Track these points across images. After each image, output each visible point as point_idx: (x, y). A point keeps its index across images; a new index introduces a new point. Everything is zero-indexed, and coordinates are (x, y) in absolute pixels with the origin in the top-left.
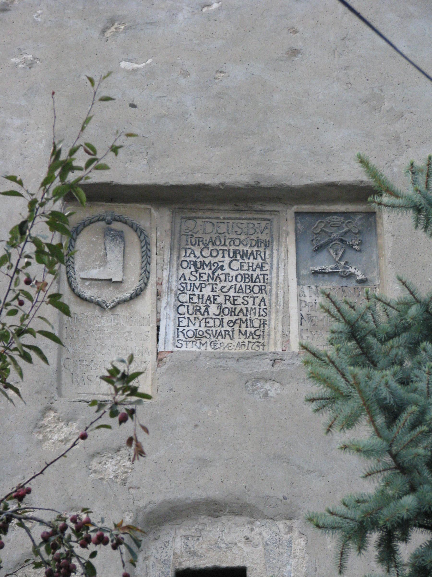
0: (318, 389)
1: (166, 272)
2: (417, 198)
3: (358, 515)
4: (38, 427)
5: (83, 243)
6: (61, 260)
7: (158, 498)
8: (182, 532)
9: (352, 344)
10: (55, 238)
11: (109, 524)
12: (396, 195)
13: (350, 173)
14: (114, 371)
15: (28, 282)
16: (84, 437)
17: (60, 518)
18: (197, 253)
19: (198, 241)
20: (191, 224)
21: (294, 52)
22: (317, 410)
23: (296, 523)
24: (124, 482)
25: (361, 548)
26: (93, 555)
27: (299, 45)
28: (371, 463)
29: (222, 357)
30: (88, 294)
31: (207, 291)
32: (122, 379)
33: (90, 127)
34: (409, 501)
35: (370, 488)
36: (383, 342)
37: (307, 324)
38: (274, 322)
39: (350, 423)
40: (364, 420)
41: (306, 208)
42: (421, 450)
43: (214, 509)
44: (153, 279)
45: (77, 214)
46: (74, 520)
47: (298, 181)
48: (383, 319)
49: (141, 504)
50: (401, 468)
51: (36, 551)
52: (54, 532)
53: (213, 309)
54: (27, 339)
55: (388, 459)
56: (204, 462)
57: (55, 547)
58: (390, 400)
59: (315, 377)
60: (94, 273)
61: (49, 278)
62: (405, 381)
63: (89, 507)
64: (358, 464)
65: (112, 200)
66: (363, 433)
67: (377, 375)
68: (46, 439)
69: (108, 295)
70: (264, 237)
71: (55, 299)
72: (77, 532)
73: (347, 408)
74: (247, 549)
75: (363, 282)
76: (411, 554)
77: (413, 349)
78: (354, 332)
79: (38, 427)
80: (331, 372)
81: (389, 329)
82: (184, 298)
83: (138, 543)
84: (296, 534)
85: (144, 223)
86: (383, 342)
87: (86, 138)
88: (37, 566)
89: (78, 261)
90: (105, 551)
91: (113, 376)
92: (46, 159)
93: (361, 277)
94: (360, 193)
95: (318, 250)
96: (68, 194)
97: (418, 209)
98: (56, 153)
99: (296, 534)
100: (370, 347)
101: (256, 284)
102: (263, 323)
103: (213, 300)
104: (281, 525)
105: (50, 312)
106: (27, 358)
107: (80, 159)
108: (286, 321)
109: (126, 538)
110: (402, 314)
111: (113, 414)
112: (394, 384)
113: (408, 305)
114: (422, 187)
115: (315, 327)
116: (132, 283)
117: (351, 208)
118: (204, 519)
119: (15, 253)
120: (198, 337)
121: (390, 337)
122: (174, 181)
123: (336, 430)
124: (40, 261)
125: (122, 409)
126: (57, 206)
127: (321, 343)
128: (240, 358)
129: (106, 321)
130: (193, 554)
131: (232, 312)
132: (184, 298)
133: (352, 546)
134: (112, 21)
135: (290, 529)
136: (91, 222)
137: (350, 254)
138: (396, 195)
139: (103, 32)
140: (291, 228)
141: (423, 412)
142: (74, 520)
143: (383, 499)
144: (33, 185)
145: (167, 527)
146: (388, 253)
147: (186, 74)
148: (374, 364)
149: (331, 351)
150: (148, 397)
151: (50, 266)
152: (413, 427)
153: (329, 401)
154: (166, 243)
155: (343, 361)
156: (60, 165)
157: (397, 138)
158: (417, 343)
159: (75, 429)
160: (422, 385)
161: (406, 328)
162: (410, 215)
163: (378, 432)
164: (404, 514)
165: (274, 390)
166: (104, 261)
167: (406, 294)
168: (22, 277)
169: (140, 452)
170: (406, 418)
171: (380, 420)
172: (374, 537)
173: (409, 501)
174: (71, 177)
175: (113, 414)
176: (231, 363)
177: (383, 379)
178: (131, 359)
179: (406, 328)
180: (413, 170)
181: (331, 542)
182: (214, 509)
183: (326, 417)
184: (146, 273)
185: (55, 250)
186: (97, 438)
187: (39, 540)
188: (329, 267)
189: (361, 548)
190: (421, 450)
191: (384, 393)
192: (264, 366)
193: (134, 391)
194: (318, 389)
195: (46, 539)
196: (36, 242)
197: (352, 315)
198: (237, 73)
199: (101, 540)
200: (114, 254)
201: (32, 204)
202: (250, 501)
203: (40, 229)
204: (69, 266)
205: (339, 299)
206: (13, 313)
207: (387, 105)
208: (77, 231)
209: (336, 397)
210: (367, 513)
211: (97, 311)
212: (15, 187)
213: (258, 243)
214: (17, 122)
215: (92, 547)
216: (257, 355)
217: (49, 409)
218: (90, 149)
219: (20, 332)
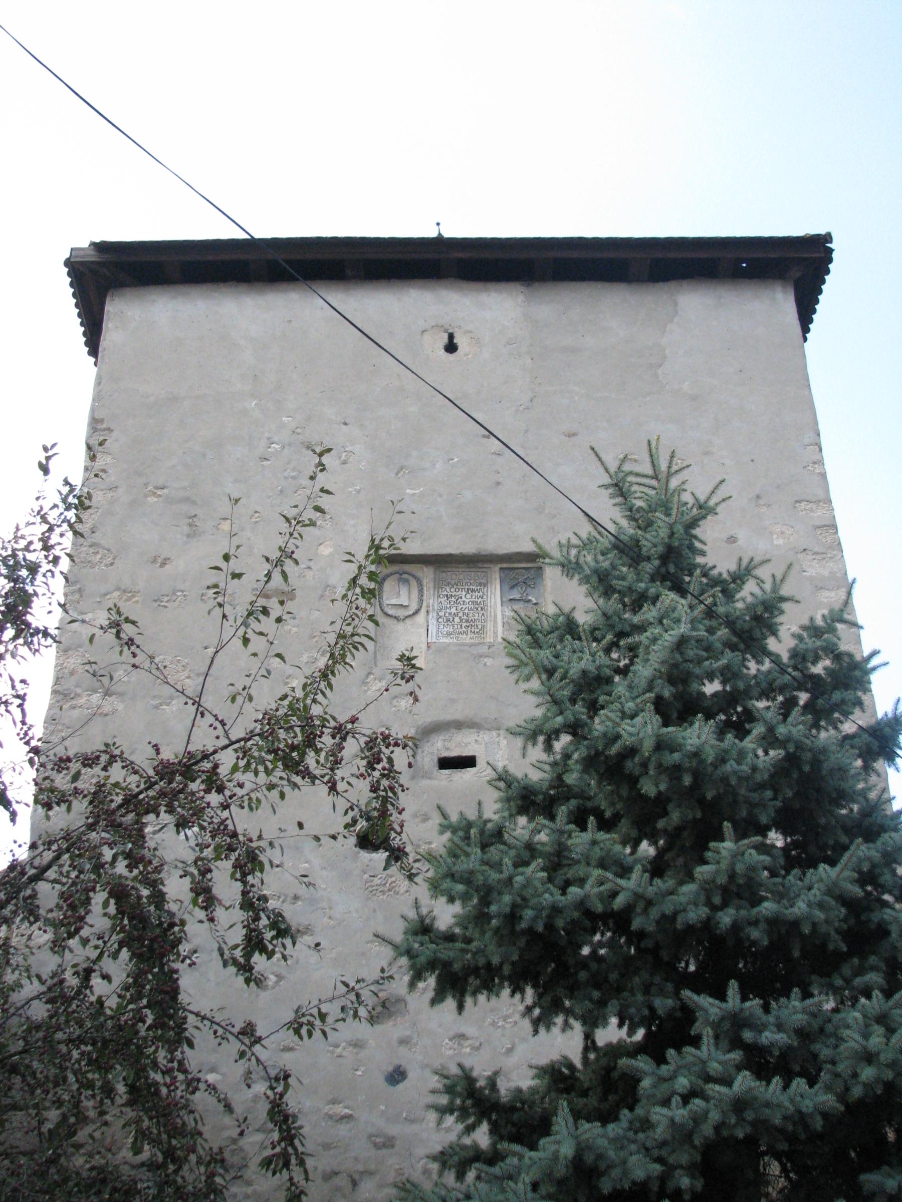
0: (511, 661)
1: (431, 600)
2: (562, 559)
3: (533, 727)
4: (364, 683)
5: (387, 586)
6: (375, 596)
7: (428, 720)
8: (442, 737)
9: (529, 637)
10: (372, 585)
11: (400, 736)
12: (551, 558)
13: (527, 547)
14: (403, 656)
15: (357, 608)
16: (387, 690)
17: (374, 733)
18: (447, 590)
19: (449, 584)
20: (444, 575)
21: (498, 483)
22: (740, 559)
23: (502, 732)
24: (410, 712)
25: (534, 744)
26: (392, 752)
27: (501, 480)
28: (540, 700)
29: (463, 645)
30: (390, 612)
31: (453, 610)
32: (407, 660)
33: (391, 527)
34: (559, 719)
35: (539, 713)
36: (545, 636)
37: (506, 627)
38: (489, 626)
39: (528, 679)
40: (535, 676)
41: (505, 565)
42: (565, 693)
43: (459, 725)
44: (425, 604)
45: (383, 570)
46: (382, 734)
47: (501, 551)
48: (545, 623)
49: (420, 723)
50: (556, 702)
51: (362, 750)
52: (371, 741)
53: (457, 620)
54: (356, 639)
55: (549, 698)
56: (453, 701)
57: (372, 748)
58: (549, 666)
59: (510, 655)
60: (394, 601)
61: (368, 606)
62: (557, 656)
63: (707, 541)
64: (533, 700)
65: (402, 563)
66: (535, 683)
67: (542, 652)
68: (369, 689)
69: (401, 613)
70: (483, 581)
71: (371, 618)
72: (384, 740)
73: (526, 671)
74: (476, 746)
75: (535, 604)
76: (714, 732)
77: (561, 639)
78: (530, 631)
79: (364, 683)
80: (518, 652)
81: (548, 629)
82: (442, 614)
83: (416, 746)
84: (502, 737)
85: (419, 574)
86: (545, 636)
87: (390, 532)
88: (362, 759)
89: (385, 596)
90: (398, 750)
91: (402, 658)
92: (368, 544)
93: (534, 601)
94: (531, 557)
95: (512, 587)
96: (378, 560)
97: (563, 566)
98: (373, 541)
99: (502, 737)
100: (538, 638)
101: (480, 607)
102: (483, 627)
103: (456, 615)
104: (494, 733)
105: (370, 625)
106: (356, 648)
107: (386, 544)
108: (495, 626)
109: (410, 744)
110: (556, 620)
111: (402, 678)
112: (551, 658)
113: (559, 616)
114: (565, 553)
115: (511, 628)
116: (414, 606)
117: (529, 565)
118: (453, 730)
119: (350, 593)
120: (449, 634)
121: (550, 633)
122: (435, 552)
123: (520, 682)
124: (363, 597)
125: (407, 676)
126: (373, 568)
127: (512, 638)
128: (471, 645)
129: (400, 627)
130: (447, 749)
131: (467, 621)
132: (442, 614)
133: (530, 744)
134: (402, 468)
135: (499, 735)
136: (391, 574)
137: (529, 590)
138: (551, 558)
139: (397, 474)
140: (497, 576)
141: (566, 672)
142: (382, 734)
143: (546, 718)
144: (360, 556)
145: (433, 735)
146: (549, 589)
147: (441, 496)
148: (541, 648)
149: (518, 641)
150: (421, 669)
151: (369, 600)
152: (561, 680)
153: (516, 668)
154: (431, 585)
155: (524, 646)
156: (375, 546)
157: (553, 528)
158: (563, 636)
159: (383, 684)
160: (566, 658)
161: (557, 629)
162: (560, 568)
163: (542, 683)
164: (557, 726)
165: (489, 661)
166: (398, 595)
167: (557, 611)
168: (354, 606)
169: (416, 700)
170: (557, 675)
171: (544, 676)
172: (541, 739)
173: (559, 719)
174: (382, 552)
175: (402, 678)
176: (467, 648)
177: (545, 655)
178: (412, 649)
179: (557, 629)
180: (560, 545)
181: (519, 742)
182: (459, 725)
183: (515, 676)
184: (421, 601)
185: (372, 591)
186: (394, 690)
187: (363, 745)
188: (518, 597)
189: (534, 744)
190: (565, 693)
191: (546, 662)
192: (484, 649)
193: (413, 666)
194: (511, 661)
195: (367, 743)
196: (361, 587)
197: (529, 621)
198: (468, 495)
199: (396, 744)
200: (404, 591)
201: (360, 567)
202: (477, 720)
203: (363, 580)
204: (381, 598)
205: (523, 615)
206: (349, 624)
207: (547, 511)
208: (384, 579)
209: (522, 664)
210: (537, 726)
211: (395, 621)
212: (351, 558)
213: (480, 584)
214: (352, 522)
215: (391, 748)
216: (480, 644)
217: (370, 673)
218: (391, 539)
219: (353, 635)
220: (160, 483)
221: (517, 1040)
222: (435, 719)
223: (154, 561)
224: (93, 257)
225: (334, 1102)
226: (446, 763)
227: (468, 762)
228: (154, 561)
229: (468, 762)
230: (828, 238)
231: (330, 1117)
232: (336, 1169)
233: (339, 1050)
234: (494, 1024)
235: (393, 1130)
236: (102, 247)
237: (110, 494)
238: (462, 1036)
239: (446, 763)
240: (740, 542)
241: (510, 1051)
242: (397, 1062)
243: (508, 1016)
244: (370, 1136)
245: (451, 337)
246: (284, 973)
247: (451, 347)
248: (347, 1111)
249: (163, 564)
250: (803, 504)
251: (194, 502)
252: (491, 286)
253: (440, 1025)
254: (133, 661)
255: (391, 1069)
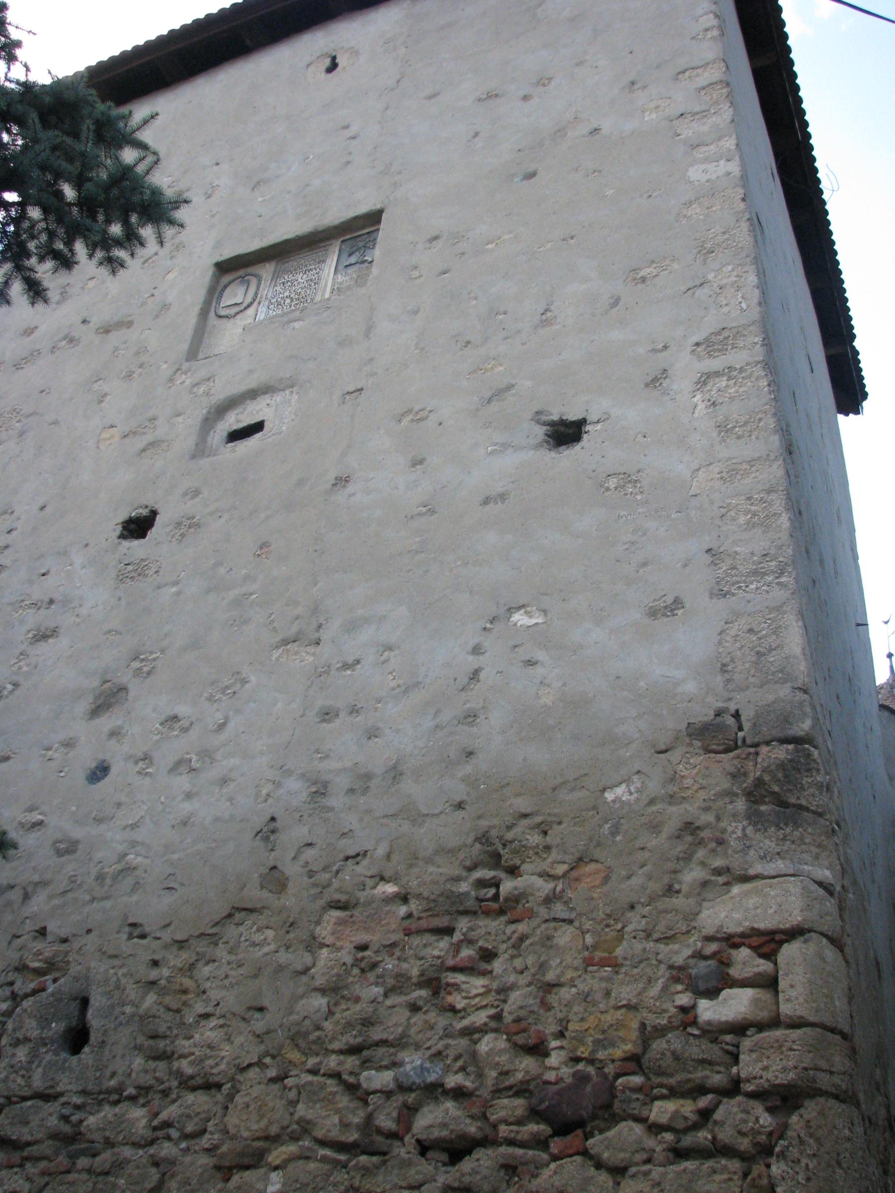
43: (253, 394)
136: (233, 281)
221: (231, 713)
222: (229, 394)
225: (31, 809)
226: (236, 436)
232: (12, 882)
233: (50, 753)
235: (78, 833)
239: (236, 436)
240: (603, 132)
241: (222, 727)
242: (101, 757)
243: (227, 687)
244: (57, 842)
248: (41, 817)
250: (687, 74)
253: (154, 710)
255: (94, 765)
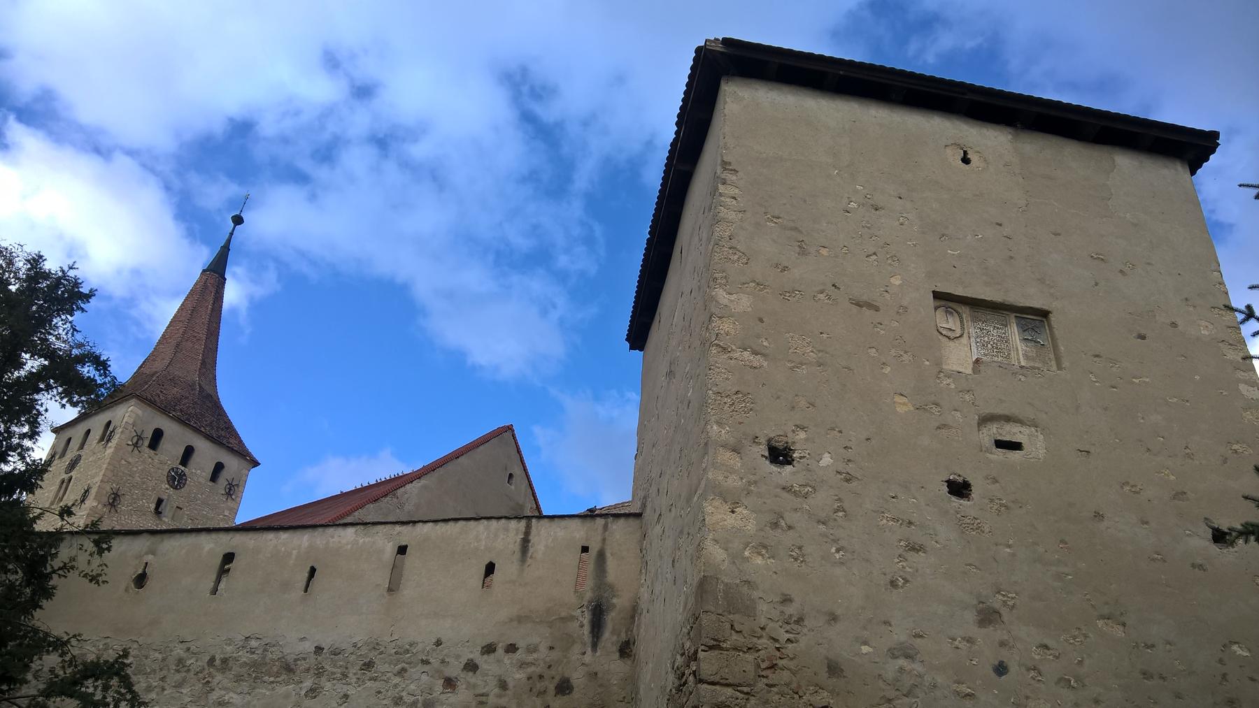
43: (1008, 419)
69: (949, 334)
129: (951, 344)
202: (1020, 417)
220: (776, 214)
223: (777, 266)
224: (720, 48)
226: (1000, 444)
227: (1016, 446)
228: (777, 266)
229: (1016, 446)
230: (1215, 135)
231: (958, 693)
234: (1066, 641)
236: (727, 42)
237: (740, 215)
238: (1046, 647)
239: (1000, 444)
245: (965, 152)
246: (909, 578)
247: (966, 160)
249: (783, 270)
251: (800, 232)
252: (989, 125)
254: (188, 645)
